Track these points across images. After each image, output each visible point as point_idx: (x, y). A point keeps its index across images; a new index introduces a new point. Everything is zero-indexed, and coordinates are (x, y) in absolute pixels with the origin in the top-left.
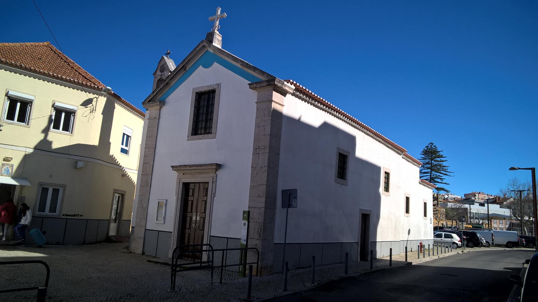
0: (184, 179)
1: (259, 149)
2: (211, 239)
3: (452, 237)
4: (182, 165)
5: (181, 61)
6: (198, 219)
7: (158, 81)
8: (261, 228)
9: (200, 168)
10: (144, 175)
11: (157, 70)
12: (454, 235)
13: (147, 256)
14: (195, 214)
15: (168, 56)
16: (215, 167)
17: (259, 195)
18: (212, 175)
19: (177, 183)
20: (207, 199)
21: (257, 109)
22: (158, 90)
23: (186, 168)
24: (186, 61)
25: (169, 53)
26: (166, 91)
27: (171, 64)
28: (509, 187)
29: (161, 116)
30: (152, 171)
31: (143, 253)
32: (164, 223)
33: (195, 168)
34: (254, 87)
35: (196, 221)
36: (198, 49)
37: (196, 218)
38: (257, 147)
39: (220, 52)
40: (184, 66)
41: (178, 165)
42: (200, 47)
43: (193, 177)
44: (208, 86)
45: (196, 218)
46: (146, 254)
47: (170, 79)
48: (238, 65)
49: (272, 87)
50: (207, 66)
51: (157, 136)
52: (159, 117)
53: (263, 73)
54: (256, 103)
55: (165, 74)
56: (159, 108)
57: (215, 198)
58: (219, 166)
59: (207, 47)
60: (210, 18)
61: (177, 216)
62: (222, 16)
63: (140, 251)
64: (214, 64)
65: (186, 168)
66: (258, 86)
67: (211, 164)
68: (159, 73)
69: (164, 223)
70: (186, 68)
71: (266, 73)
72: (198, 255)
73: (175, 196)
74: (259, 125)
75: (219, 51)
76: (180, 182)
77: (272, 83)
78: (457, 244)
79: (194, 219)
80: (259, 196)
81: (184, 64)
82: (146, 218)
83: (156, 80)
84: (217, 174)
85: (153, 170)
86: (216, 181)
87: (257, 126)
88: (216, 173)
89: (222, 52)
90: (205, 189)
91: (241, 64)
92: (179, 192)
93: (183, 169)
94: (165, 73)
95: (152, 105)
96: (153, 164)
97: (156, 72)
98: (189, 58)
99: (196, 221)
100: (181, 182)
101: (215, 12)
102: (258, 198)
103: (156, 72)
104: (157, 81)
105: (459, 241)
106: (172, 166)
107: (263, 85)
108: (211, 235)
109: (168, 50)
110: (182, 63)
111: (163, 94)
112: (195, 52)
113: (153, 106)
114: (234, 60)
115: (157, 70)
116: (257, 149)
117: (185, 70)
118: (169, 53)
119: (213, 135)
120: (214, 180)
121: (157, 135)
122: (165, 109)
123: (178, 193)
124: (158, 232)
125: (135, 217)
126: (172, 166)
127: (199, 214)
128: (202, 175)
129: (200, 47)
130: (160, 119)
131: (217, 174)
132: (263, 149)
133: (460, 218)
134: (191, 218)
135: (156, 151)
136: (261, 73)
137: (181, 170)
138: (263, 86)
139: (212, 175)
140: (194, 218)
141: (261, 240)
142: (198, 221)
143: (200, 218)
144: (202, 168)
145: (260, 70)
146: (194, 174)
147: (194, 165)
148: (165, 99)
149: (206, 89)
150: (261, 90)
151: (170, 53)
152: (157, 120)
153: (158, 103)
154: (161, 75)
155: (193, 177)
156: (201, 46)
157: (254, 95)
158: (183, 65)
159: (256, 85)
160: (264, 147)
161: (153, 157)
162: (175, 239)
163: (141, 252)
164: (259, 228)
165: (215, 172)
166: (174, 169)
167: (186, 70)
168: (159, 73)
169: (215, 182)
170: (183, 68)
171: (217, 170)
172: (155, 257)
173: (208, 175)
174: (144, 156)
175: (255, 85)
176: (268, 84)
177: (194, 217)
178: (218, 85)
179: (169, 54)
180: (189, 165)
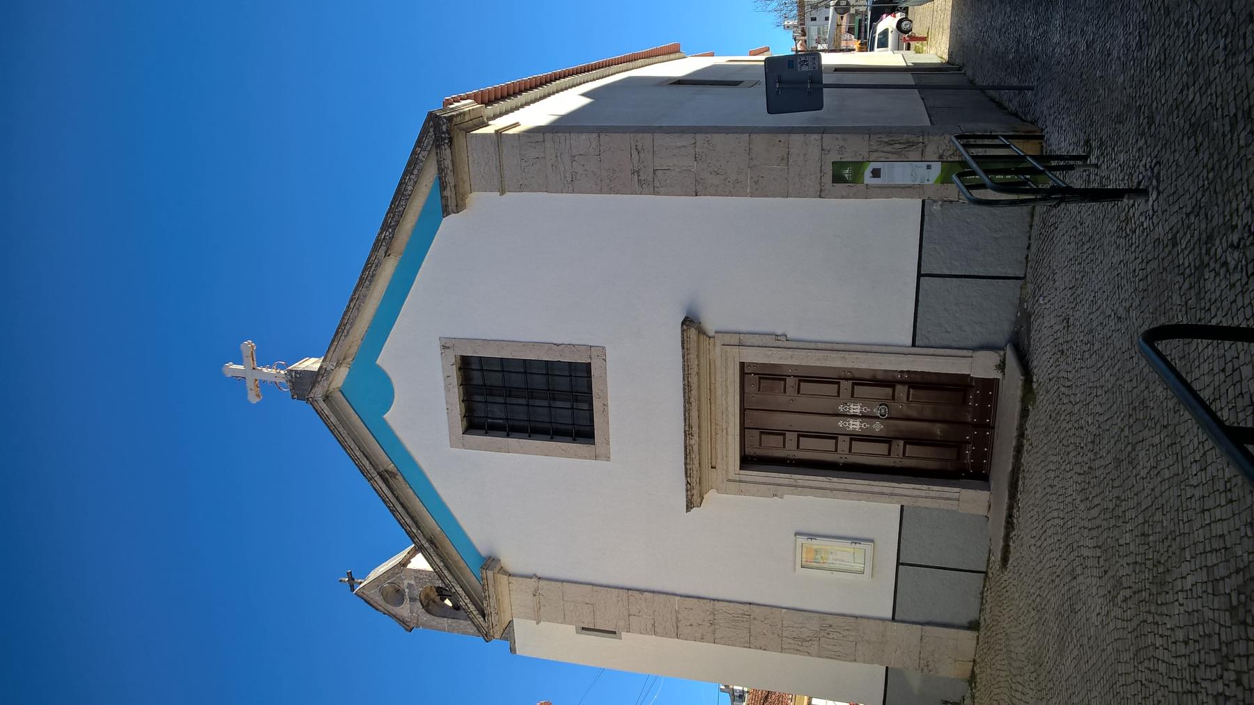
0: (731, 468)
1: (641, 173)
2: (922, 345)
3: (885, 33)
4: (686, 464)
5: (367, 481)
6: (856, 409)
7: (428, 611)
8: (888, 144)
9: (694, 392)
10: (714, 632)
11: (394, 616)
12: (881, 27)
13: (981, 610)
14: (840, 424)
15: (359, 581)
16: (693, 333)
17: (783, 159)
18: (718, 348)
19: (741, 492)
20: (794, 376)
21: (521, 188)
22: (450, 577)
23: (696, 448)
24: (367, 463)
25: (351, 579)
26: (454, 552)
27: (380, 570)
28: (769, 8)
29: (530, 571)
30: (703, 598)
31: (974, 626)
32: (872, 541)
33: (694, 414)
34: (453, 196)
35: (863, 416)
36: (333, 419)
37: (854, 416)
38: (636, 177)
39: (345, 331)
40: (381, 476)
41: (685, 483)
42: (327, 411)
43: (724, 427)
44: (447, 390)
45: (854, 416)
46: (973, 615)
47: (418, 527)
48: (388, 269)
49: (458, 135)
50: (384, 392)
51: (593, 585)
52: (531, 578)
53: (413, 165)
54: (502, 192)
55: (410, 586)
56: (504, 579)
57: (789, 336)
58: (690, 322)
59: (331, 389)
60: (253, 399)
61: (849, 487)
62: (250, 355)
63: (967, 639)
64: (381, 365)
65: (696, 448)
66: (450, 179)
67: (683, 348)
68: (404, 610)
69: (872, 541)
70: (387, 471)
71: (414, 152)
72: (975, 401)
73: (781, 497)
74: (570, 180)
75: (343, 338)
76: (740, 481)
77: (444, 128)
78: (900, 22)
79: (858, 427)
80: (786, 159)
81: (375, 474)
82: (856, 617)
83: (426, 617)
84: (716, 332)
85: (699, 598)
86: (735, 333)
87: (571, 185)
88: (712, 334)
89: (345, 325)
90: (765, 383)
91: (382, 252)
92: (770, 484)
93: (696, 462)
94: (406, 582)
95: (492, 602)
96: (681, 596)
97: (402, 622)
98: (358, 453)
99: (863, 416)
100: (737, 478)
101: (240, 380)
102: (791, 161)
103: (402, 622)
104: (429, 616)
105: (894, 16)
106: (689, 508)
107: (448, 162)
108: (910, 342)
109: (341, 581)
110: (370, 479)
111: (462, 564)
112: (341, 429)
113: (498, 601)
114: (373, 276)
115: (394, 616)
116: (642, 178)
117: (393, 475)
118: (351, 579)
119: (593, 357)
120: (735, 339)
121: (589, 584)
122: (511, 559)
123: (773, 484)
124: (900, 567)
125: (855, 663)
126: (689, 508)
127: (841, 408)
128: (719, 392)
129: (327, 411)
130: (539, 574)
131: (716, 332)
132: (642, 155)
133: (841, 11)
134: (855, 437)
135: (642, 586)
136: (415, 172)
137: (700, 470)
138: (453, 161)
139: (718, 348)
140: (855, 425)
141: (926, 141)
142: (866, 410)
143: (855, 404)
144: (694, 386)
145: (405, 174)
146: (713, 425)
147: (685, 415)
148: (478, 554)
149: (456, 393)
150: (466, 177)
151: (350, 575)
152: (542, 583)
153: (490, 573)
154: (412, 599)
155: (724, 427)
156: (323, 405)
157: (480, 201)
158: (378, 478)
159: (448, 188)
160: (635, 153)
161: (657, 597)
162: (923, 493)
163: (968, 632)
164: (888, 148)
165: (710, 337)
166: (696, 499)
167: (395, 470)
168: (404, 610)
169: (740, 340)
170: (387, 479)
171: (701, 331)
172: (986, 573)
173: (718, 363)
174: (655, 633)
175: (447, 193)
176: (447, 141)
177: (851, 427)
178: (444, 347)
179: (353, 579)
180: (685, 436)
